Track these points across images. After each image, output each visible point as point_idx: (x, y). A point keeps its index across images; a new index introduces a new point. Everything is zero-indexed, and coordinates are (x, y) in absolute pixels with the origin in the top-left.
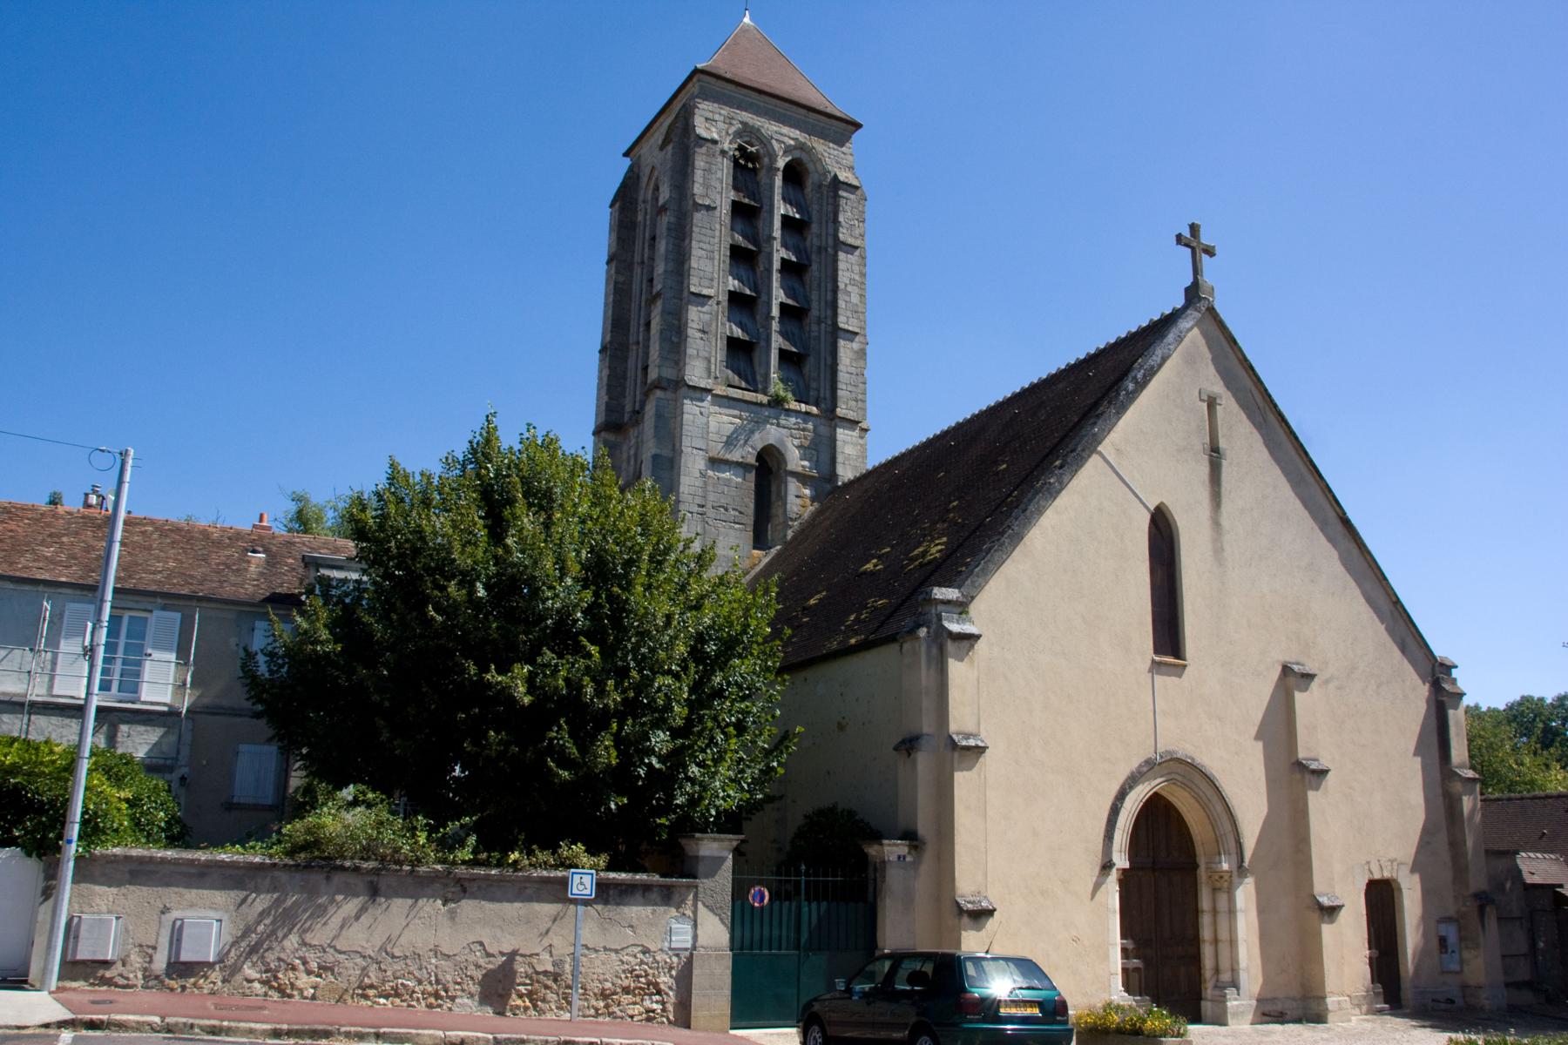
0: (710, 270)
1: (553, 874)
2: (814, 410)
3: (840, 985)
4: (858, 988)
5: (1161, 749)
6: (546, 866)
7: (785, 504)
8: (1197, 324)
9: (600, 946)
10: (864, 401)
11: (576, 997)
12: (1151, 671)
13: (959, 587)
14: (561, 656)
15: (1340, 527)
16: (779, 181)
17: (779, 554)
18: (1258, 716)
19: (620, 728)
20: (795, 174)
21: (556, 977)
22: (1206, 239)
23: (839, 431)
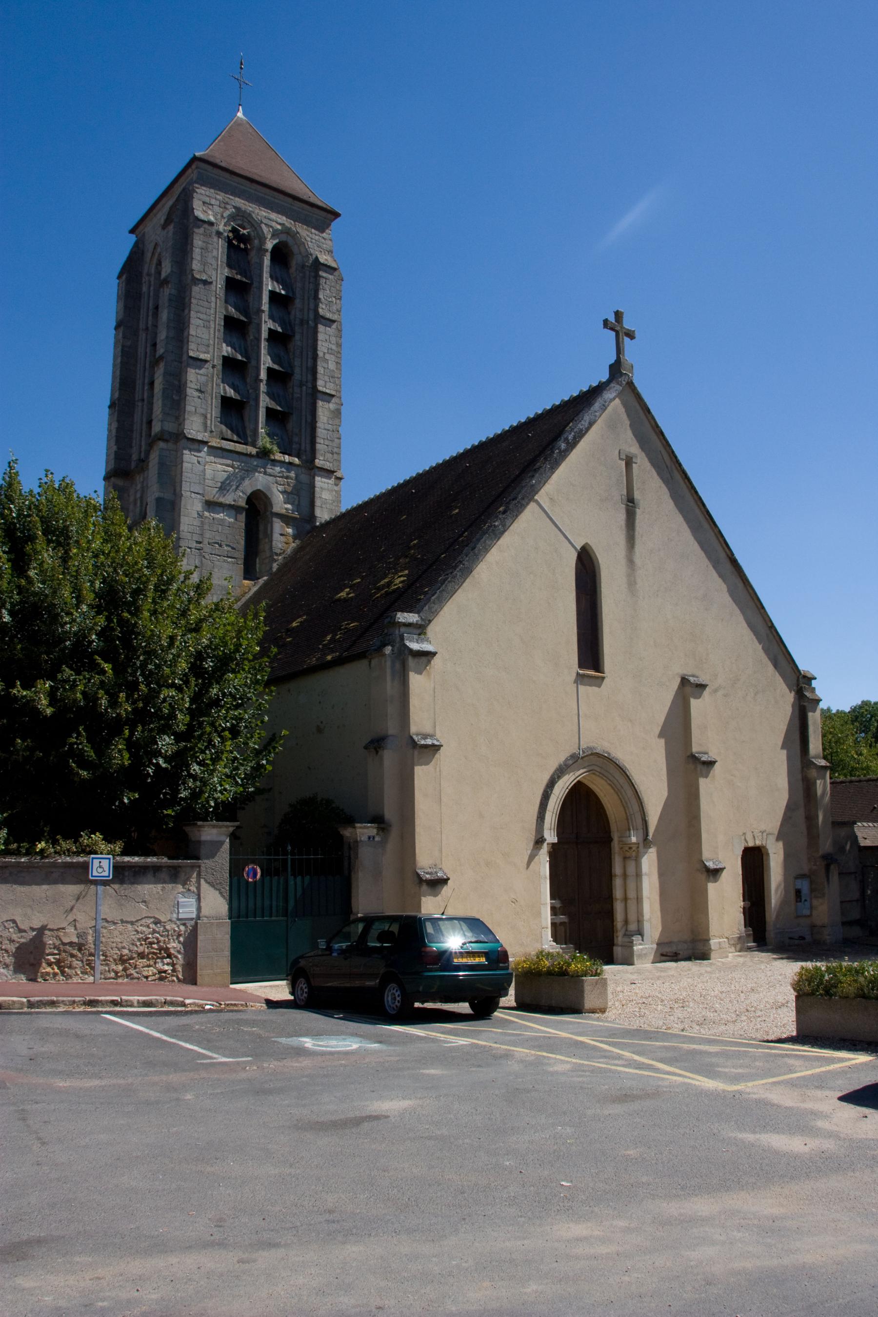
0: (206, 338)
1: (75, 860)
2: (296, 461)
3: (322, 944)
4: (336, 946)
5: (584, 745)
6: (69, 853)
7: (271, 541)
8: (618, 396)
9: (117, 919)
10: (339, 454)
11: (98, 963)
12: (576, 682)
13: (418, 612)
14: (78, 673)
15: (728, 565)
16: (267, 261)
17: (266, 584)
18: (661, 718)
19: (132, 734)
20: (281, 255)
21: (80, 947)
22: (627, 324)
23: (317, 479)
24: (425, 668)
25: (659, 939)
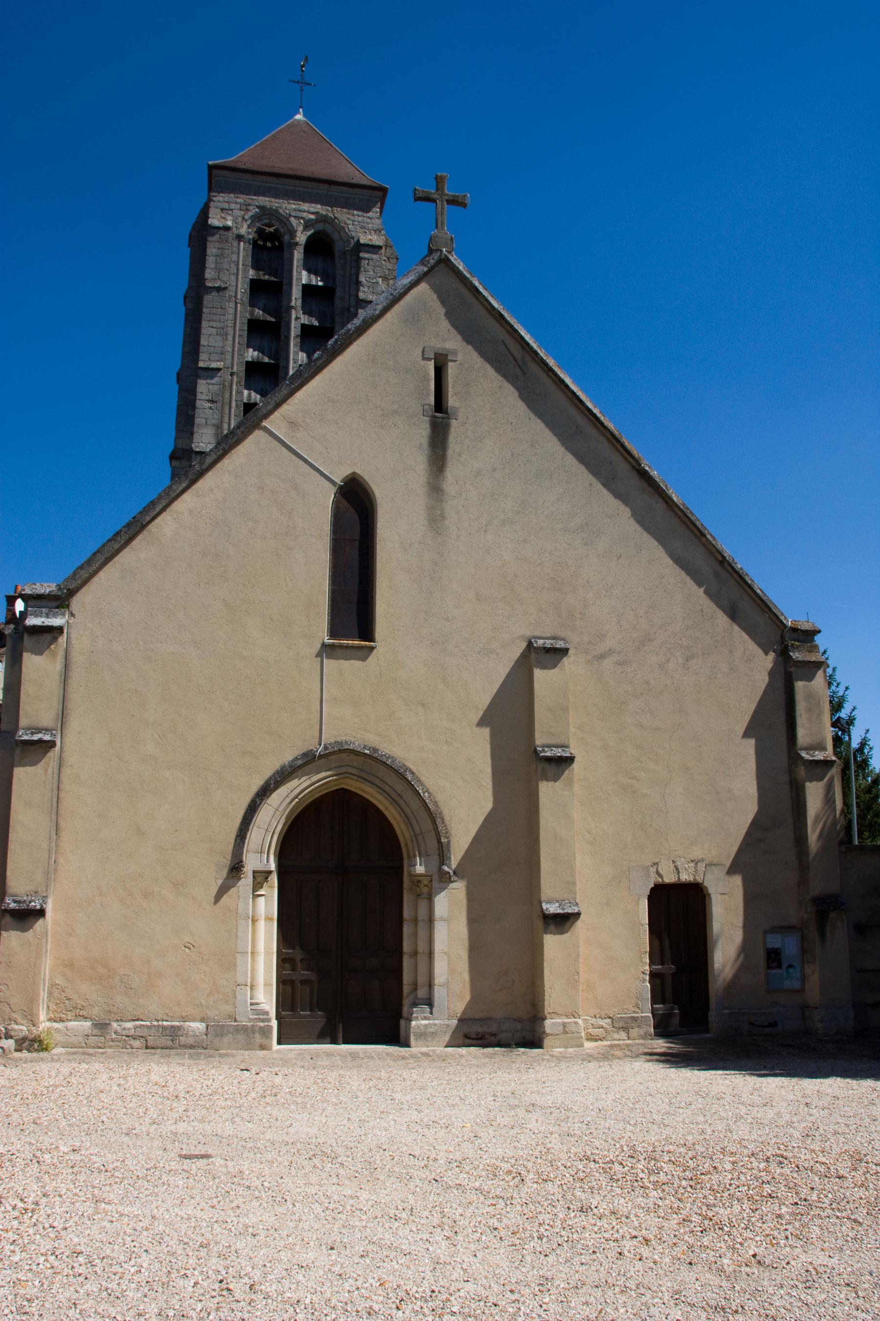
5: (329, 737)
12: (319, 655)
15: (635, 481)
24: (49, 647)
25: (464, 1013)
